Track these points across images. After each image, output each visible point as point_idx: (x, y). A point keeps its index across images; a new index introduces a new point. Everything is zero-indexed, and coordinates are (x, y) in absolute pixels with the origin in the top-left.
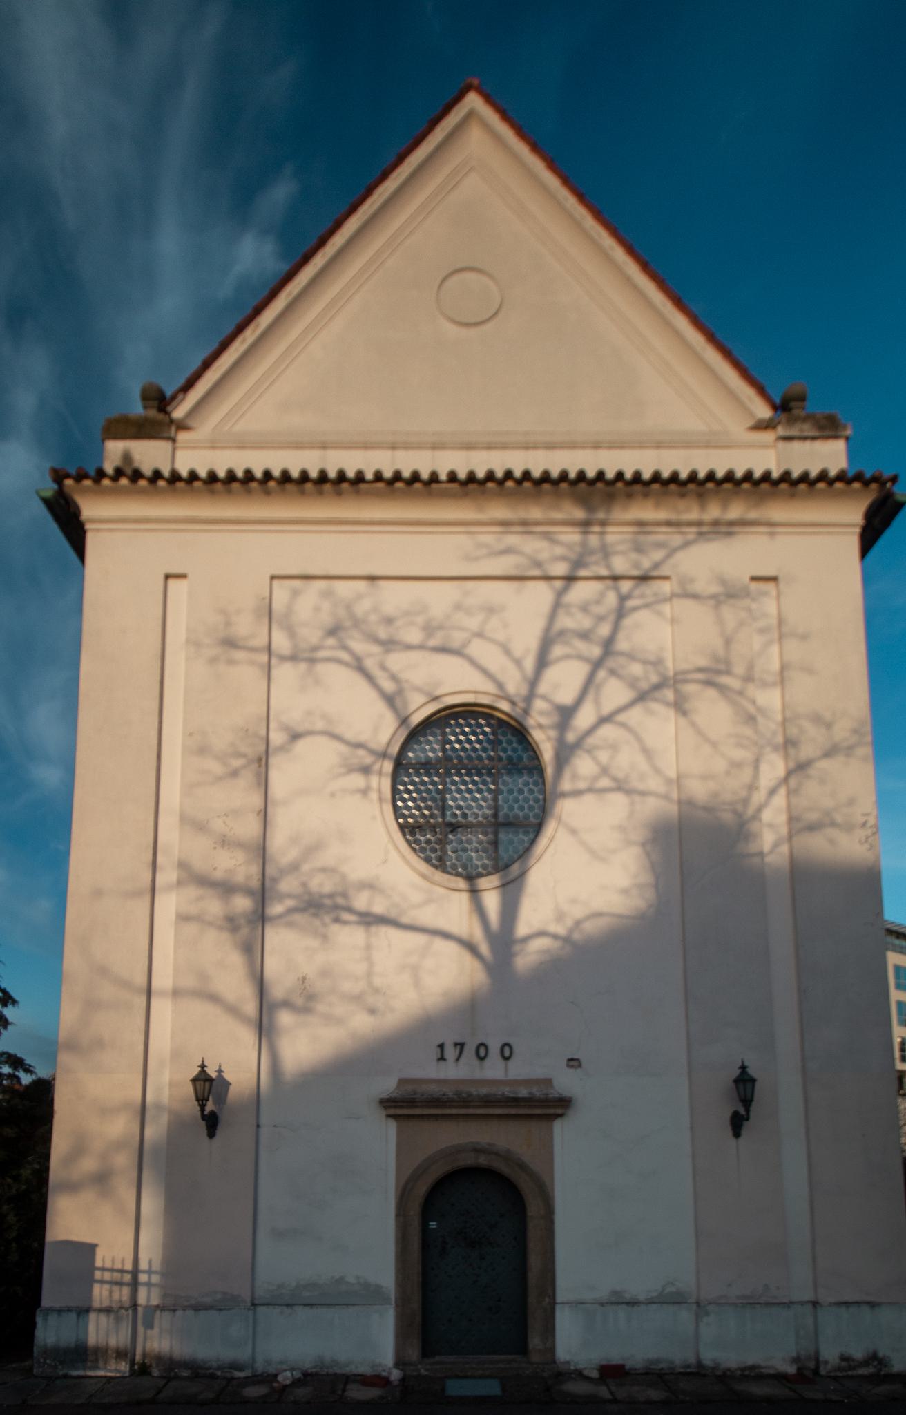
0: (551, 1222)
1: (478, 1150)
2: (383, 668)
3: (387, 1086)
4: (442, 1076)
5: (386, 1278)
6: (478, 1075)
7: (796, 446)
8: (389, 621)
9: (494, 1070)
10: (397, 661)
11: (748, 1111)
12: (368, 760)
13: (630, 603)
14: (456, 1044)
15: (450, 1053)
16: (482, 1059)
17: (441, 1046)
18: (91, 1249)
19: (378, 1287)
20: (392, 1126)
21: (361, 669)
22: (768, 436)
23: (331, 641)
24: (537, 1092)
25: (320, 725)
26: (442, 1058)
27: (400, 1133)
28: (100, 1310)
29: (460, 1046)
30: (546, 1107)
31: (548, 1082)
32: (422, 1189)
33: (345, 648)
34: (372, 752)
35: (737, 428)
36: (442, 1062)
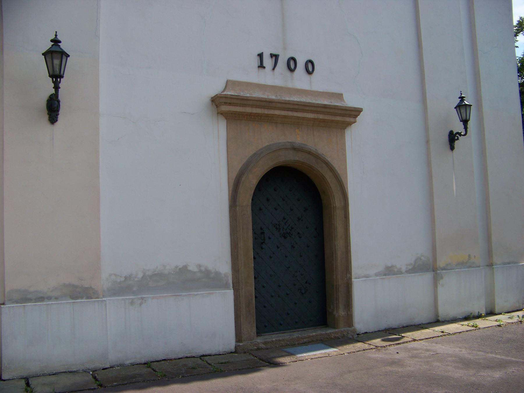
1: (296, 149)
5: (224, 266)
9: (299, 80)
11: (466, 128)
14: (272, 55)
15: (268, 62)
16: (292, 70)
17: (261, 56)
19: (218, 274)
26: (261, 66)
29: (275, 57)
30: (339, 117)
31: (340, 96)
32: (252, 180)
36: (261, 70)
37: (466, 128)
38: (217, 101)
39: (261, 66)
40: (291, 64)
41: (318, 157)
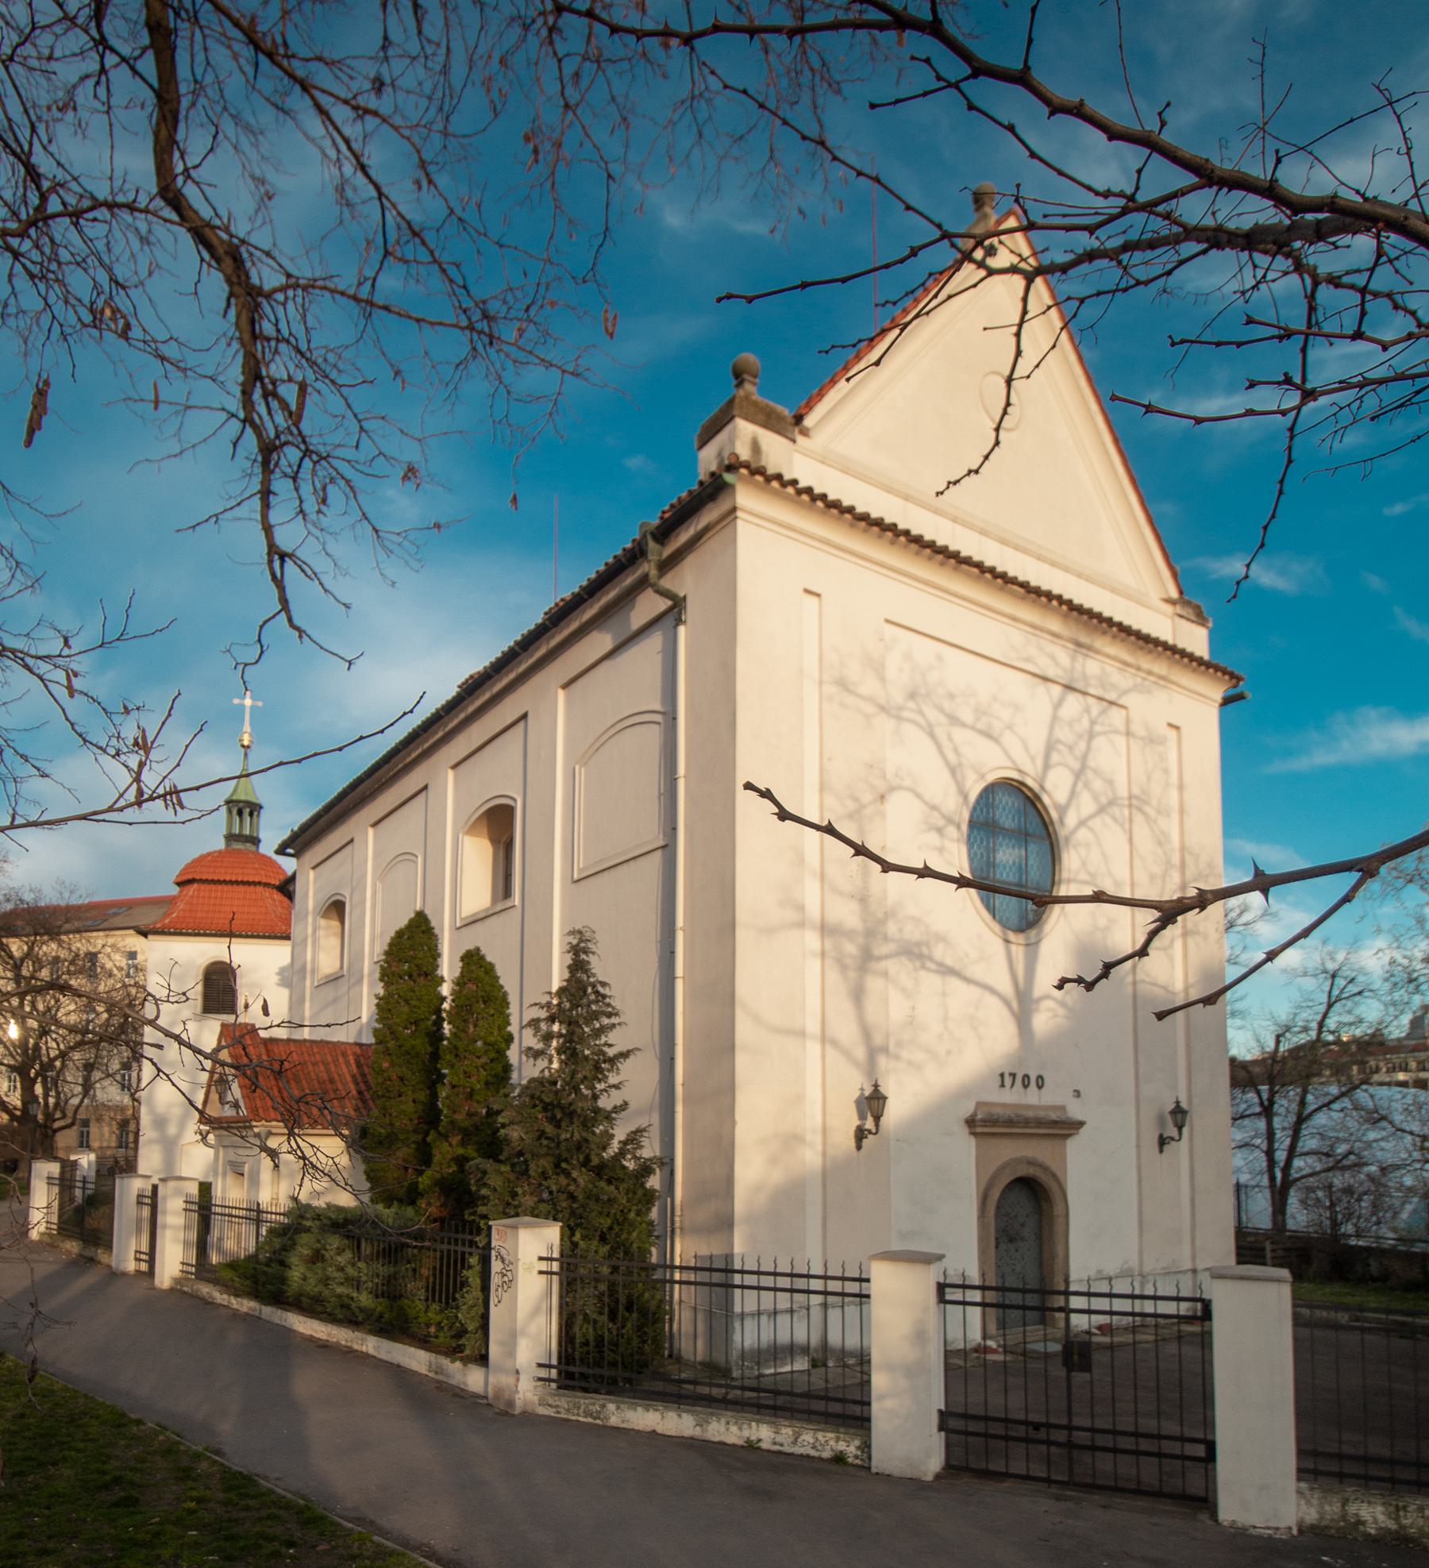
0: (1067, 1225)
1: (1031, 1163)
2: (950, 739)
3: (968, 1108)
4: (1002, 1101)
6: (1024, 1101)
7: (1184, 622)
8: (952, 696)
10: (960, 735)
11: (1180, 1134)
12: (941, 823)
13: (1097, 728)
15: (1008, 1081)
17: (1002, 1075)
18: (940, 1412)
20: (973, 1140)
21: (932, 735)
22: (1169, 609)
23: (911, 704)
24: (1053, 1116)
25: (907, 783)
26: (1003, 1085)
27: (978, 1147)
28: (1362, 1340)
29: (1013, 1075)
30: (1063, 1128)
31: (1063, 1108)
32: (996, 1194)
33: (921, 713)
34: (944, 816)
35: (1155, 596)
37: (877, 1125)
38: (971, 1122)
39: (1003, 1085)
40: (1026, 1081)
41: (1041, 1166)
